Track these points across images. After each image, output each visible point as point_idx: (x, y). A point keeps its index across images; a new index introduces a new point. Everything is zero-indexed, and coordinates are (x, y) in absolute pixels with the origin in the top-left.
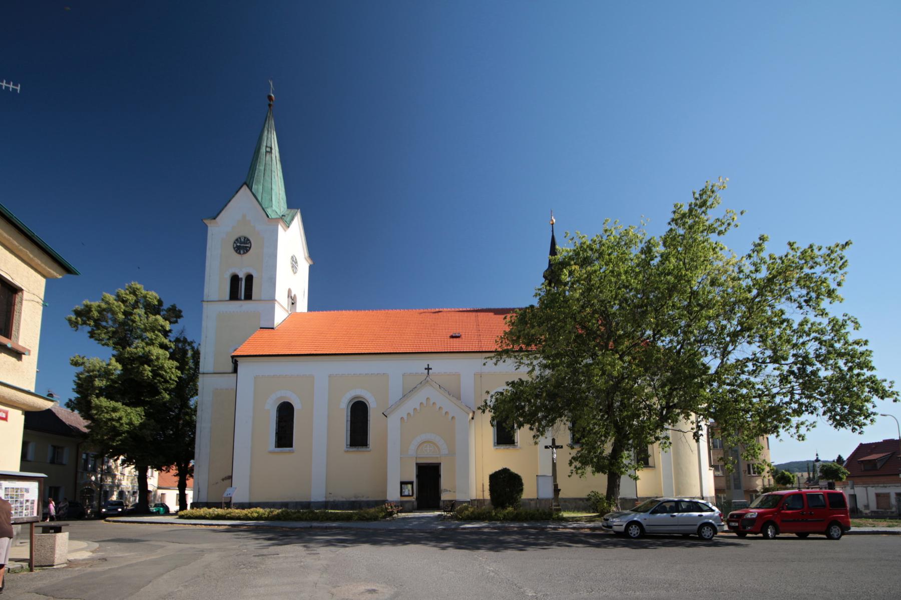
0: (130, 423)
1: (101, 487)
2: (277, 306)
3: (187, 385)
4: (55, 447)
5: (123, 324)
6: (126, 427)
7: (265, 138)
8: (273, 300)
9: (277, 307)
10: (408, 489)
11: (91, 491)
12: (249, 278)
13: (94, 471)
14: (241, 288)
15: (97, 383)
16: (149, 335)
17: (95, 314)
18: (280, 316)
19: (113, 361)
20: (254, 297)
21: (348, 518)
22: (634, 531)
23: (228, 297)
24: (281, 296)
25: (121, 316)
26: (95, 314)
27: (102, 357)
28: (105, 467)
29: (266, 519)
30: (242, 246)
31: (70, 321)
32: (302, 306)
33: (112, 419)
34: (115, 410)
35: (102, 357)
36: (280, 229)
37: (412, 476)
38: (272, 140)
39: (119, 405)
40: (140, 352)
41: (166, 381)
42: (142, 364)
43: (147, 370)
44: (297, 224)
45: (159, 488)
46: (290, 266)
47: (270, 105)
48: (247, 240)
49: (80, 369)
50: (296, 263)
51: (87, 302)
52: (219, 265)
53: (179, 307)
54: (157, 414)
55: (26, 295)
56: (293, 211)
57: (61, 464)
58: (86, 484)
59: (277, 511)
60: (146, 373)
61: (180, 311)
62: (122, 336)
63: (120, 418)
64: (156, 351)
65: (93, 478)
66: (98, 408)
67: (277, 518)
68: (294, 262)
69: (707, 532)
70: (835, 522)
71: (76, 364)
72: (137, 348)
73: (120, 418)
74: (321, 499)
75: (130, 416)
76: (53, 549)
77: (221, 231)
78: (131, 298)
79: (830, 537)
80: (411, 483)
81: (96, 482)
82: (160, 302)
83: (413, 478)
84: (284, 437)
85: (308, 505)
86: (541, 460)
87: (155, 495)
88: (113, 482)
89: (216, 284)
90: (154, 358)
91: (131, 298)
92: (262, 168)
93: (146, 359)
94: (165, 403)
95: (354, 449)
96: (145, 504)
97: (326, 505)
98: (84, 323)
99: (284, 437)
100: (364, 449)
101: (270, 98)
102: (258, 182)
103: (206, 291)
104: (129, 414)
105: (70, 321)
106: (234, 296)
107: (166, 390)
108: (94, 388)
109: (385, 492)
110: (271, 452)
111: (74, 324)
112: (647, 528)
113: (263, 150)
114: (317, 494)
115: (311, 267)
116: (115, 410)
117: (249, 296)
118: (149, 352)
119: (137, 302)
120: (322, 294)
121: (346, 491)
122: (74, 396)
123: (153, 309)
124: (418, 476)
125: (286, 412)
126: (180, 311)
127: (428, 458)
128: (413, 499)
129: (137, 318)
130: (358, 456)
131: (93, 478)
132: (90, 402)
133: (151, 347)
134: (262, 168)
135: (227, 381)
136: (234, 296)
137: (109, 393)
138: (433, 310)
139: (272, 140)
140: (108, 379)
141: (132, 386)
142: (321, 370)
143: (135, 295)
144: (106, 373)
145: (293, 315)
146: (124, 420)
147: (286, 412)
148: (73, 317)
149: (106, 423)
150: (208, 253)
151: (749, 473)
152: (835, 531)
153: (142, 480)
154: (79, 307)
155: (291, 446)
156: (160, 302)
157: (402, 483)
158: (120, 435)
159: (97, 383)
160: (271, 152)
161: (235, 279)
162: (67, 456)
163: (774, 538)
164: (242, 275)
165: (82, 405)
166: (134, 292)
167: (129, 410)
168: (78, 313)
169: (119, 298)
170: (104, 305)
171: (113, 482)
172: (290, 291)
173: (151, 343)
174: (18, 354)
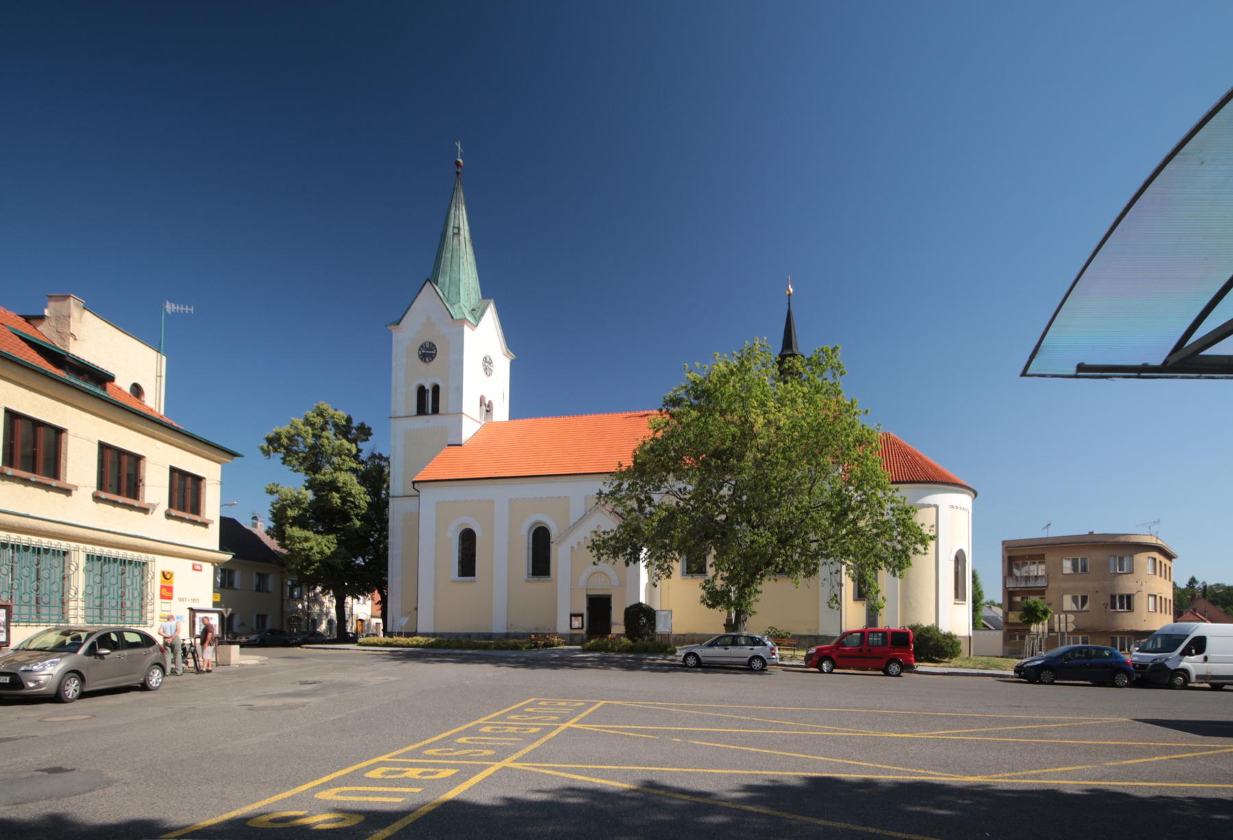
0: (321, 553)
1: (309, 615)
2: (464, 418)
3: (379, 507)
4: (258, 574)
5: (313, 447)
6: (318, 557)
7: (452, 216)
8: (459, 413)
9: (465, 420)
10: (577, 623)
11: (299, 619)
12: (436, 389)
13: (301, 599)
14: (429, 401)
15: (290, 513)
16: (336, 460)
17: (285, 441)
18: (469, 429)
19: (304, 491)
20: (441, 411)
21: (486, 647)
22: (691, 661)
23: (415, 412)
24: (470, 406)
25: (310, 441)
26: (285, 441)
27: (295, 484)
28: (311, 594)
29: (422, 647)
30: (427, 353)
31: (262, 449)
32: (501, 413)
33: (304, 549)
34: (307, 540)
35: (295, 484)
36: (467, 329)
37: (583, 608)
38: (461, 218)
39: (310, 534)
40: (328, 478)
41: (357, 507)
42: (330, 491)
43: (336, 498)
44: (490, 318)
45: (372, 617)
46: (482, 369)
47: (458, 173)
48: (432, 347)
49: (275, 497)
50: (490, 363)
51: (277, 429)
52: (407, 375)
53: (367, 425)
54: (352, 543)
55: (208, 482)
56: (485, 302)
57: (267, 591)
58: (292, 612)
59: (433, 640)
60: (334, 501)
61: (369, 429)
62: (313, 460)
63: (311, 548)
64: (343, 477)
65: (300, 606)
66: (291, 538)
67: (431, 646)
68: (487, 363)
69: (757, 664)
70: (895, 660)
71: (271, 492)
72: (326, 473)
73: (311, 548)
74: (504, 631)
75: (320, 544)
76: (229, 655)
77: (407, 336)
78: (319, 421)
79: (887, 674)
80: (582, 615)
81: (302, 610)
82: (349, 420)
83: (584, 611)
84: (467, 566)
85: (489, 636)
86: (674, 596)
87: (369, 625)
88: (321, 610)
89: (405, 400)
90: (340, 485)
91: (319, 421)
92: (449, 255)
93: (332, 486)
94: (356, 530)
95: (535, 578)
96: (341, 634)
97: (507, 636)
98: (275, 451)
99: (467, 566)
100: (543, 578)
101: (458, 164)
102: (445, 273)
103: (393, 406)
104: (319, 544)
105: (262, 449)
106: (421, 410)
107: (357, 515)
108: (287, 518)
109: (555, 628)
110: (454, 582)
111: (266, 453)
112: (703, 660)
113: (450, 232)
114: (499, 627)
115: (513, 365)
116: (307, 540)
117: (436, 410)
118: (268, 533)
119: (326, 423)
120: (527, 396)
121: (525, 624)
122: (272, 524)
123: (344, 430)
124: (588, 608)
125: (468, 538)
126: (369, 429)
127: (599, 589)
128: (583, 631)
129: (326, 441)
130: (540, 585)
131: (300, 606)
132: (284, 532)
133: (338, 474)
134: (449, 255)
135: (409, 505)
136: (421, 410)
137: (300, 522)
138: (642, 413)
139: (461, 218)
140: (300, 508)
141: (323, 514)
142: (501, 494)
143: (323, 417)
144: (297, 503)
145: (489, 427)
146: (316, 549)
147: (468, 538)
148: (265, 445)
149: (299, 553)
150: (394, 364)
151: (1113, 607)
152: (895, 668)
153: (340, 608)
154: (271, 434)
155: (473, 575)
156: (349, 420)
157: (572, 615)
158: (313, 564)
159: (290, 513)
160: (459, 234)
161: (422, 391)
162: (271, 583)
163: (830, 672)
164: (428, 386)
165: (278, 532)
166: (321, 414)
167: (319, 538)
168: (270, 441)
169: (308, 422)
170: (293, 432)
171: (321, 610)
172: (482, 399)
173: (338, 469)
174: (205, 525)
